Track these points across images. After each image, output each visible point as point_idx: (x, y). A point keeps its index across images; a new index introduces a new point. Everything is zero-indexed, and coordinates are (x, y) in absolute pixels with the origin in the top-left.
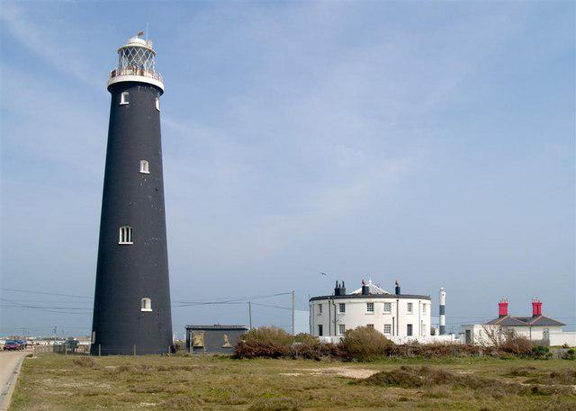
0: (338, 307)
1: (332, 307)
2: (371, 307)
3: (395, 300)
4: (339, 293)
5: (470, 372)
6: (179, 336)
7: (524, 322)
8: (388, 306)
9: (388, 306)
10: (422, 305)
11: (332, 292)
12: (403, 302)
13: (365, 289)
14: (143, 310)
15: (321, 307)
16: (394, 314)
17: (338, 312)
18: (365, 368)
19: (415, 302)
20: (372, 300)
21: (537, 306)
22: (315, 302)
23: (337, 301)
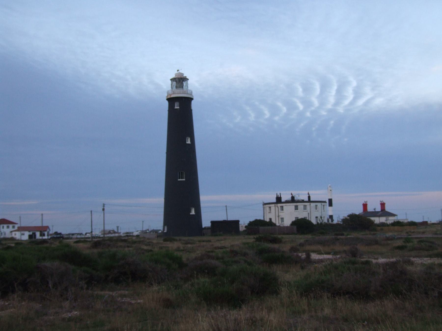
0: (279, 208)
1: (277, 208)
2: (296, 208)
3: (309, 204)
4: (279, 200)
5: (237, 243)
6: (206, 223)
7: (375, 214)
8: (305, 207)
9: (305, 207)
10: (322, 206)
11: (275, 201)
12: (313, 205)
13: (293, 198)
14: (191, 214)
15: (91, 213)
16: (309, 212)
17: (280, 211)
18: (81, 234)
19: (319, 204)
20: (298, 204)
21: (383, 205)
22: (267, 206)
23: (279, 205)
